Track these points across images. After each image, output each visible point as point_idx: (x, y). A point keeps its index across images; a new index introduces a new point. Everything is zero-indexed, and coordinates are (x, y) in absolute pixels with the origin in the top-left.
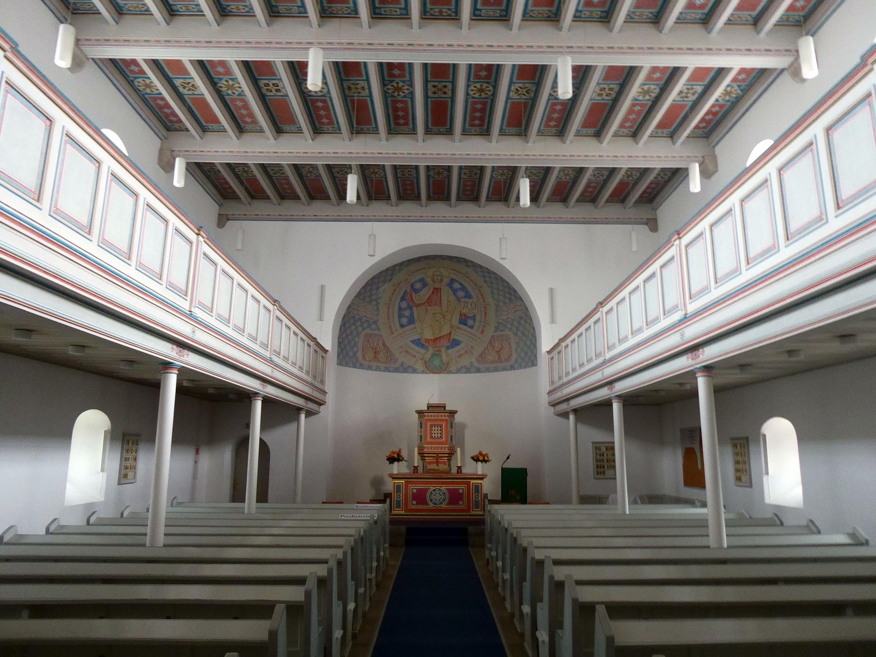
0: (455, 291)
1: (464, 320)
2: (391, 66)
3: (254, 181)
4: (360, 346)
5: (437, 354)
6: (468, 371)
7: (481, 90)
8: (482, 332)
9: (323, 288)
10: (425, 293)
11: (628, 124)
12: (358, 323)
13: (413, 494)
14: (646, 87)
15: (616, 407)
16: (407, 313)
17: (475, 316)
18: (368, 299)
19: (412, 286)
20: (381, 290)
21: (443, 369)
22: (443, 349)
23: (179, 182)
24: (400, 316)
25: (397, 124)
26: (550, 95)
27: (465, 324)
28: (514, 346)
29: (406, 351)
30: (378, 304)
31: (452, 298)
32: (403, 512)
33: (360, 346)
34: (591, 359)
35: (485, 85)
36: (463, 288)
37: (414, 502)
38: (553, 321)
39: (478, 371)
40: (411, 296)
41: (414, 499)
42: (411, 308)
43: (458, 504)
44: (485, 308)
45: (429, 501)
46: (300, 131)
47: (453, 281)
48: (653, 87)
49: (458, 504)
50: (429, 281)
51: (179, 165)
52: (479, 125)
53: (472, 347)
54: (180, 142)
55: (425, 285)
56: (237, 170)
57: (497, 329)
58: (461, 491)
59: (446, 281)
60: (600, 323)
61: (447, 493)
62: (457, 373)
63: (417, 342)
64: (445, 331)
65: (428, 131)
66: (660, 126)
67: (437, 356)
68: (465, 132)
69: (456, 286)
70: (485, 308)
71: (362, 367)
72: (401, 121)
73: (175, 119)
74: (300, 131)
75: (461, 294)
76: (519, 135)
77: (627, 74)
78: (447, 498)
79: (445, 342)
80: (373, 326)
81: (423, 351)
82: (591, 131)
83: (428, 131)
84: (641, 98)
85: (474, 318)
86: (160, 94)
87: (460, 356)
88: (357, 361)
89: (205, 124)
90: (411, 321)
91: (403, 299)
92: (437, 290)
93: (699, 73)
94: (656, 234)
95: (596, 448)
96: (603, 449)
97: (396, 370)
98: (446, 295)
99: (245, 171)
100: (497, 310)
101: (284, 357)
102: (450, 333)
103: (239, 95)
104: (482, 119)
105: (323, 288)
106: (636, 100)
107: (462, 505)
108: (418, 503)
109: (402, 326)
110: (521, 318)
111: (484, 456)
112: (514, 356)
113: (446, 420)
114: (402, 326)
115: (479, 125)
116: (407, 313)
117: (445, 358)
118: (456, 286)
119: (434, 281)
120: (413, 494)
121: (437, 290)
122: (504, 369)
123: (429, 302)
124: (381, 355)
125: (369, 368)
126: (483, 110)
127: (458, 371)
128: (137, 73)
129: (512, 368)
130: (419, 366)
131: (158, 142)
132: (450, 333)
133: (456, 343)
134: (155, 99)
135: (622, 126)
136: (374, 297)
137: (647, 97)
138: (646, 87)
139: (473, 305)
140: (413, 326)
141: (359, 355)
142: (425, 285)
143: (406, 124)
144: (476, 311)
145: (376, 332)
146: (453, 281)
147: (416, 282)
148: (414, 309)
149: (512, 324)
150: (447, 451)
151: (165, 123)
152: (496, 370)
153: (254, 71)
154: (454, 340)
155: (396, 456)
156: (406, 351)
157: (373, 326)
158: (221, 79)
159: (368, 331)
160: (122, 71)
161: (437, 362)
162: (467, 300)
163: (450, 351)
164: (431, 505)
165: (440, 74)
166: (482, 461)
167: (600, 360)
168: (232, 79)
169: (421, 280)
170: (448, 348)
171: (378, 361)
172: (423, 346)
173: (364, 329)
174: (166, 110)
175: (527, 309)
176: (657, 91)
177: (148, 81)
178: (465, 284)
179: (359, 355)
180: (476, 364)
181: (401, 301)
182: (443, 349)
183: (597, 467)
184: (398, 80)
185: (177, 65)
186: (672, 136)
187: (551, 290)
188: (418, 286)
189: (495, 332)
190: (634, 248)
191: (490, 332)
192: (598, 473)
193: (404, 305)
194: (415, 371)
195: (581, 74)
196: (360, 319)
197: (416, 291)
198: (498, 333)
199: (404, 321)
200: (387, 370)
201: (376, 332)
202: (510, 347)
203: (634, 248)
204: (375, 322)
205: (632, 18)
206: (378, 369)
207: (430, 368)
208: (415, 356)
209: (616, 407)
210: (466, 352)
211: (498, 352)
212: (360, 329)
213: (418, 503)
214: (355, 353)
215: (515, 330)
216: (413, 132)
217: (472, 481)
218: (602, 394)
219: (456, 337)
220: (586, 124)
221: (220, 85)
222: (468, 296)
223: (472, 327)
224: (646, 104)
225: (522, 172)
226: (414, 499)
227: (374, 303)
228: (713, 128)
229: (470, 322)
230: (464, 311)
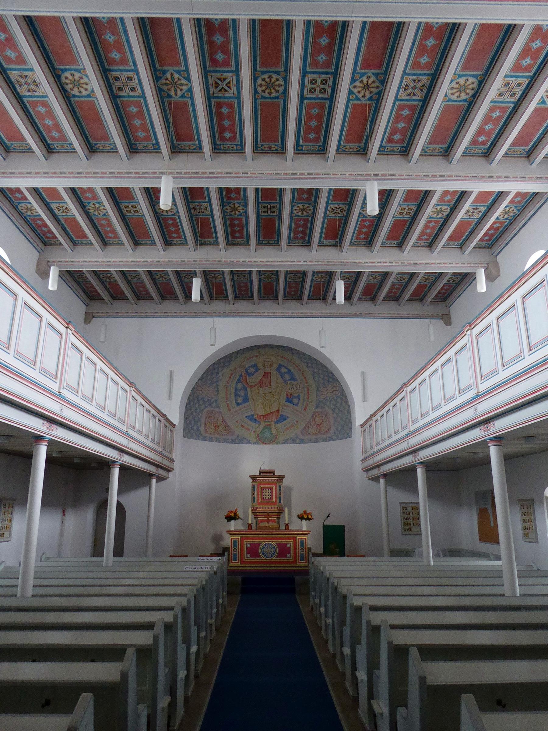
0: (282, 375)
1: (289, 399)
2: (228, 190)
3: (115, 285)
4: (203, 421)
5: (268, 427)
6: (294, 442)
7: (303, 210)
8: (305, 409)
9: (171, 372)
10: (258, 377)
11: (482, 139)
12: (201, 402)
13: (248, 548)
14: (439, 208)
15: (420, 472)
16: (242, 393)
17: (299, 395)
18: (209, 382)
19: (246, 370)
20: (220, 374)
21: (272, 440)
22: (273, 423)
23: (52, 286)
24: (237, 395)
25: (234, 237)
26: (360, 213)
27: (291, 402)
28: (332, 422)
29: (242, 425)
30: (218, 386)
31: (280, 380)
32: (239, 564)
33: (203, 421)
34: (398, 431)
35: (306, 206)
36: (289, 372)
37: (249, 555)
38: (365, 399)
39: (302, 441)
40: (246, 378)
41: (248, 553)
42: (245, 389)
43: (286, 557)
44: (308, 389)
45: (261, 554)
46: (153, 244)
47: (280, 366)
48: (444, 207)
49: (286, 557)
50: (261, 366)
51: (54, 272)
52: (302, 238)
53: (297, 422)
54: (53, 253)
55: (257, 369)
56: (101, 276)
57: (317, 406)
58: (288, 545)
59: (275, 366)
60: (405, 400)
61: (276, 547)
62: (284, 443)
63: (251, 418)
64: (274, 409)
65: (259, 243)
66: (451, 239)
67: (268, 429)
68: (290, 244)
69: (283, 370)
70: (308, 389)
71: (204, 439)
72: (237, 235)
73: (96, 293)
74: (153, 244)
75: (287, 377)
76: (335, 245)
77: (422, 198)
78: (277, 552)
79: (274, 418)
80: (214, 405)
81: (256, 425)
82: (395, 242)
83: (259, 243)
84: (435, 216)
85: (298, 397)
86: (39, 215)
87: (288, 429)
88: (200, 434)
89: (75, 239)
90: (246, 400)
91: (239, 381)
92: (267, 374)
93: (483, 196)
94: (449, 327)
95: (403, 507)
96: (410, 509)
97: (233, 442)
98: (275, 378)
99: (107, 277)
100: (318, 391)
101: (138, 430)
102: (278, 410)
103: (104, 215)
104: (304, 233)
105: (171, 372)
106: (431, 218)
107: (289, 557)
108: (251, 557)
109: (238, 404)
110: (338, 397)
111: (308, 514)
112: (333, 429)
113: (275, 484)
114: (238, 404)
115: (302, 238)
116: (242, 393)
117: (274, 431)
118: (283, 370)
119: (264, 366)
120: (248, 548)
121: (267, 374)
122: (324, 440)
123: (261, 383)
124: (221, 428)
125: (210, 440)
126: (304, 226)
127: (285, 442)
128: (20, 199)
129: (331, 439)
130: (253, 438)
131: (36, 255)
132: (278, 410)
133: (283, 418)
134: (34, 220)
135: (419, 238)
136: (214, 380)
137: (440, 216)
138: (439, 208)
139: (298, 386)
140: (247, 404)
141: (202, 429)
142: (257, 369)
143: (242, 237)
144: (300, 391)
145: (217, 409)
146: (280, 366)
147: (249, 367)
148: (248, 389)
149: (331, 402)
150: (276, 510)
151: (42, 238)
152: (317, 441)
153: (116, 196)
154: (282, 416)
155: (233, 515)
156: (242, 425)
157: (214, 405)
158: (89, 203)
159: (209, 408)
160: (10, 197)
161: (267, 434)
162: (293, 382)
163: (279, 425)
164: (263, 558)
165: (269, 196)
166: (306, 519)
167: (406, 432)
168: (99, 203)
169: (255, 365)
170: (277, 422)
171: (218, 434)
172: (255, 421)
173: (206, 407)
174: (43, 229)
175: (343, 390)
176: (448, 210)
177: (29, 205)
178: (289, 368)
179: (202, 429)
180: (301, 436)
181: (237, 383)
182: (273, 423)
183: (405, 524)
184: (234, 202)
185: (53, 192)
186: (421, 300)
187: (363, 374)
188: (251, 370)
189: (316, 408)
190: (432, 339)
191: (312, 408)
192: (405, 530)
193: (240, 386)
194: (249, 442)
195: (386, 196)
196: (203, 398)
197: (250, 375)
198: (319, 410)
199: (240, 400)
200: (225, 441)
201: (217, 409)
202: (329, 421)
203: (432, 339)
204: (216, 401)
205: (426, 152)
206: (218, 441)
207: (262, 440)
208: (248, 430)
209: (420, 472)
210: (292, 426)
211: (319, 425)
212: (203, 407)
213: (251, 557)
214: (198, 427)
215: (332, 406)
216: (247, 243)
217: (298, 537)
218: (476, 434)
219: (284, 414)
220: (390, 237)
221: (88, 207)
222: (293, 378)
223: (297, 405)
224: (439, 221)
225: (338, 275)
226: (248, 553)
227: (215, 385)
228: (495, 241)
229: (295, 401)
230: (290, 391)
